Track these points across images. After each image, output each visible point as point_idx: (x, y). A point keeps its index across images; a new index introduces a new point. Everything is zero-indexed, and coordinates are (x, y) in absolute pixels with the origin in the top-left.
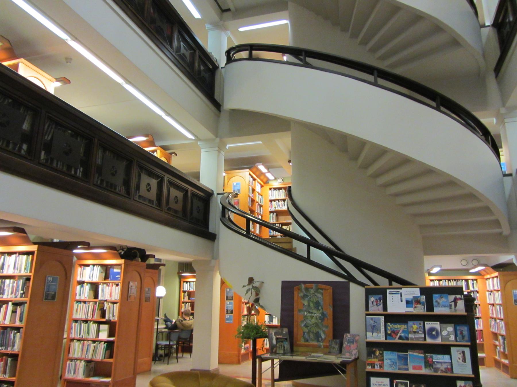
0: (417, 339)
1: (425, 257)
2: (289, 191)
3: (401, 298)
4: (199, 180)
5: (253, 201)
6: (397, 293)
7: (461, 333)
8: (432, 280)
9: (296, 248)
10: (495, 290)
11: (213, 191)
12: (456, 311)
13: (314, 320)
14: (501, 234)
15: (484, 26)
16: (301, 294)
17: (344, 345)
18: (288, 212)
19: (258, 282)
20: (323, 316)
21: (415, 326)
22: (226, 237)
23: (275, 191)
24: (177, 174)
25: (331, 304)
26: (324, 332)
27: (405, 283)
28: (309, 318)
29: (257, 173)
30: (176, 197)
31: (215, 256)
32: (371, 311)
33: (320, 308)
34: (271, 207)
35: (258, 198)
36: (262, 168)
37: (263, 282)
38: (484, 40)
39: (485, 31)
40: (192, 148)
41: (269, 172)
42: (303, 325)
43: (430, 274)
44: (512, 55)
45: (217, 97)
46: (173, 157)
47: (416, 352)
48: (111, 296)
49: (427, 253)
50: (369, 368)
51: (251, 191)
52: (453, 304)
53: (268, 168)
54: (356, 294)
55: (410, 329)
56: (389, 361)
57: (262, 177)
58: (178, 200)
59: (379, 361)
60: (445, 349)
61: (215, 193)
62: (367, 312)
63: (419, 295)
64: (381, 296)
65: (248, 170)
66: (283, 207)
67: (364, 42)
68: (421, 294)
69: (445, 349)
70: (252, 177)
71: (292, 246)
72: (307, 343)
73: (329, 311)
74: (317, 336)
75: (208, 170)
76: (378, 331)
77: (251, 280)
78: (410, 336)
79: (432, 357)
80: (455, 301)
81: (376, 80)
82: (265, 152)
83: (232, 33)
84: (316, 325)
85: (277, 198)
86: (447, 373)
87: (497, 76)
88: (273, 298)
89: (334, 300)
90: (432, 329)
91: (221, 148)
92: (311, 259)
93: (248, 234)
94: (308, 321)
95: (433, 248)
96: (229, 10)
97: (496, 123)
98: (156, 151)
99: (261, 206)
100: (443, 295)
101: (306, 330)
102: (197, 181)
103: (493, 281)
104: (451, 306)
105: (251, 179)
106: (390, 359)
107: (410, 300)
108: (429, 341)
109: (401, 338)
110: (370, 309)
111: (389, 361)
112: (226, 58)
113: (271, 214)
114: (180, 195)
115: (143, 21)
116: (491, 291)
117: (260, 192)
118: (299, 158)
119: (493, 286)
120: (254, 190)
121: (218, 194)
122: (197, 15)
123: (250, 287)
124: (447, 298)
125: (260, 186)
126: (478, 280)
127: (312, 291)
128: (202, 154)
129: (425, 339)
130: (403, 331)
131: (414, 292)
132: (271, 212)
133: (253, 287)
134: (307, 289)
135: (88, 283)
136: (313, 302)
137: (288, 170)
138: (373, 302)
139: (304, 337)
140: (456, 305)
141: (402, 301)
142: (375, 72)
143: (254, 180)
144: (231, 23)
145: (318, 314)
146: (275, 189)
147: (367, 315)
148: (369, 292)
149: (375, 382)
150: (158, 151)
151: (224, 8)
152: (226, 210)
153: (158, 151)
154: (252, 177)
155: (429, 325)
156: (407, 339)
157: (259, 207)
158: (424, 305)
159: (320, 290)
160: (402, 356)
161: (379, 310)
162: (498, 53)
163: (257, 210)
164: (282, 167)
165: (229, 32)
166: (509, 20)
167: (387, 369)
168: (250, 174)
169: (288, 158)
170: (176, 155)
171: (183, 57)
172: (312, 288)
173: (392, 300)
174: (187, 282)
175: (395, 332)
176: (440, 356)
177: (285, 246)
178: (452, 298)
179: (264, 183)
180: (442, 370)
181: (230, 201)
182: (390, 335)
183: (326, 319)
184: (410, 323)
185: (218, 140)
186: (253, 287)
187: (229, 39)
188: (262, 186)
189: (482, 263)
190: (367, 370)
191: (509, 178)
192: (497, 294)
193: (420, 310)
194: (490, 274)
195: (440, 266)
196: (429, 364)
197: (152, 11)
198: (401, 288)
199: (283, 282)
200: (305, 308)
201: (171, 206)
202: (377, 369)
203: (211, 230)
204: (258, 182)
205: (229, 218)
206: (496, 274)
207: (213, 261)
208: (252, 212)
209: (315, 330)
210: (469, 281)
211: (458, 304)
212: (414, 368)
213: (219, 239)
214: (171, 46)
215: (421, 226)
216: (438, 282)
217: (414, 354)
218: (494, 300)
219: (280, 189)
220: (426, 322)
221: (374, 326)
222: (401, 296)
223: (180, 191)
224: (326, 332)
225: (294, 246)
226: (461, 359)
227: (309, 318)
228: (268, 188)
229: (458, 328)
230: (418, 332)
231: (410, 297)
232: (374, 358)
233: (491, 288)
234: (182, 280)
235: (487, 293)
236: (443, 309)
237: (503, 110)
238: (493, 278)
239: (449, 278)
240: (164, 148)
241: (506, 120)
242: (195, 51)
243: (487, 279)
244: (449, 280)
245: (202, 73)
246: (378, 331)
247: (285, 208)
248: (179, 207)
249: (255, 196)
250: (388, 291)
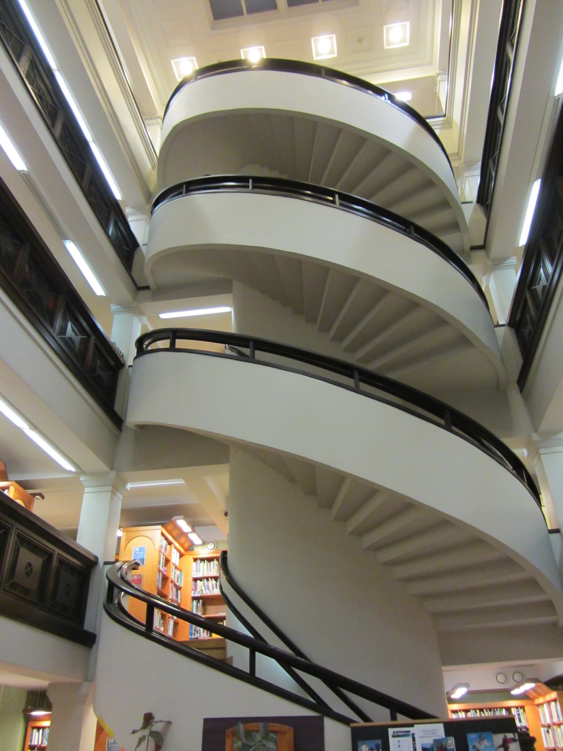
1: (444, 668)
2: (224, 559)
3: (414, 744)
4: (75, 539)
5: (165, 579)
6: (406, 734)
8: (455, 712)
9: (231, 658)
10: (554, 724)
11: (96, 558)
14: (555, 625)
15: (498, 326)
18: (224, 599)
19: (161, 721)
22: (112, 638)
23: (202, 564)
24: (39, 527)
27: (417, 715)
29: (175, 533)
30: (29, 564)
31: (89, 676)
34: (196, 589)
35: (173, 575)
36: (182, 524)
37: (169, 723)
38: (500, 343)
39: (501, 332)
40: (71, 487)
41: (194, 531)
43: (451, 701)
44: (539, 360)
45: (117, 408)
46: (38, 501)
49: (445, 663)
51: (162, 561)
53: (194, 525)
57: (183, 540)
58: (31, 570)
61: (101, 562)
63: (444, 736)
64: (379, 742)
65: (160, 527)
66: (215, 589)
67: (339, 338)
68: (447, 734)
70: (166, 539)
71: (225, 654)
75: (90, 520)
77: (148, 719)
80: (505, 744)
81: (357, 385)
82: (190, 499)
83: (149, 319)
85: (206, 575)
87: (521, 391)
91: (117, 486)
92: (257, 675)
93: (147, 632)
95: (458, 651)
96: (147, 288)
97: (528, 456)
98: (8, 488)
99: (178, 588)
100: (484, 734)
102: (72, 541)
103: (549, 707)
105: (165, 542)
107: (429, 747)
112: (135, 350)
113: (195, 602)
114: (37, 561)
115: (9, 279)
116: (549, 726)
117: (177, 564)
118: (244, 509)
119: (551, 717)
120: (167, 561)
122: (99, 290)
123: (146, 732)
124: (491, 740)
125: (178, 554)
126: (526, 708)
127: (258, 737)
128: (85, 495)
131: (434, 732)
132: (194, 598)
133: (152, 733)
134: (249, 734)
137: (223, 529)
142: (356, 374)
143: (170, 543)
144: (149, 306)
146: (202, 560)
148: (358, 736)
150: (12, 489)
151: (140, 285)
152: (116, 591)
153: (12, 489)
154: (166, 539)
157: (174, 589)
159: (271, 735)
162: (520, 361)
163: (171, 594)
164: (214, 524)
165: (145, 319)
166: (531, 318)
168: (163, 534)
169: (223, 507)
170: (43, 497)
171: (69, 342)
172: (258, 731)
173: (397, 749)
174: (39, 728)
177: (215, 654)
178: (498, 738)
179: (186, 550)
181: (124, 575)
185: (113, 474)
186: (152, 733)
187: (144, 326)
188: (181, 555)
189: (527, 677)
191: (556, 535)
192: (559, 730)
194: (543, 695)
195: (467, 685)
197: (27, 271)
198: (412, 725)
199: (206, 721)
201: (16, 579)
203: (88, 626)
204: (176, 548)
205: (119, 604)
206: (553, 695)
207: (86, 684)
208: (163, 596)
210: (512, 709)
213: (98, 643)
214: (52, 325)
215: (435, 616)
216: (463, 713)
218: (555, 742)
219: (210, 560)
222: (414, 739)
223: (37, 554)
225: (229, 655)
228: (191, 558)
233: (549, 721)
234: (32, 724)
235: (543, 730)
237: (535, 437)
238: (549, 702)
239: (480, 705)
240: (24, 485)
241: (541, 451)
242: (89, 337)
243: (538, 705)
244: (481, 710)
245: (98, 372)
247: (217, 592)
248: (32, 583)
249: (169, 571)
250: (391, 731)
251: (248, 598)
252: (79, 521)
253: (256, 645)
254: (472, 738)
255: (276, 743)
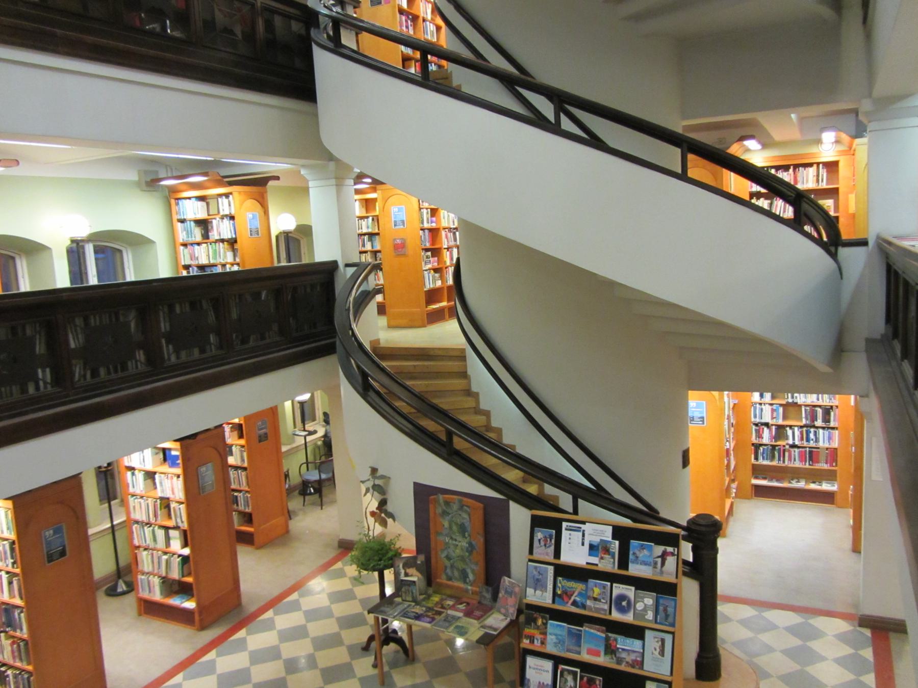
0: (598, 610)
6: (578, 530)
7: (665, 610)
12: (662, 573)
13: (458, 551)
16: (439, 510)
17: (500, 595)
20: (471, 548)
21: (596, 587)
25: (481, 531)
26: (473, 571)
28: (452, 547)
32: (536, 556)
33: (466, 534)
42: (443, 555)
47: (595, 629)
48: (173, 493)
50: (525, 643)
52: (659, 560)
54: (519, 517)
55: (590, 593)
56: (555, 636)
59: (541, 633)
60: (636, 632)
61: (341, 265)
62: (531, 557)
69: (636, 632)
72: (450, 583)
73: (479, 542)
74: (464, 576)
76: (544, 588)
77: (374, 471)
78: (589, 603)
79: (616, 640)
80: (664, 556)
84: (462, 558)
86: (633, 667)
88: (403, 502)
89: (486, 524)
90: (622, 597)
94: (450, 551)
101: (447, 563)
104: (656, 563)
106: (556, 635)
107: (595, 544)
108: (616, 616)
109: (575, 603)
110: (535, 551)
111: (553, 637)
121: (347, 265)
124: (650, 549)
129: (610, 613)
130: (580, 594)
134: (447, 503)
135: (140, 470)
136: (456, 524)
138: (539, 540)
139: (447, 574)
140: (663, 564)
141: (583, 544)
145: (464, 544)
147: (530, 560)
148: (537, 522)
149: (532, 665)
155: (619, 589)
156: (584, 607)
158: (613, 557)
160: (574, 631)
161: (547, 554)
167: (550, 649)
175: (567, 594)
176: (629, 641)
178: (659, 550)
180: (627, 662)
182: (560, 596)
183: (474, 552)
184: (592, 582)
190: (522, 645)
193: (608, 564)
196: (610, 650)
200: (445, 532)
202: (537, 646)
209: (461, 565)
211: (667, 563)
212: (590, 652)
217: (592, 631)
220: (614, 585)
221: (538, 580)
222: (583, 535)
224: (474, 571)
226: (658, 650)
227: (452, 547)
229: (661, 601)
230: (600, 601)
231: (596, 540)
232: (534, 629)
236: (643, 567)
246: (544, 588)
250: (564, 524)
251: (480, 26)
252: (250, 675)
253: (479, 66)
254: (634, 543)
255: (469, 515)
